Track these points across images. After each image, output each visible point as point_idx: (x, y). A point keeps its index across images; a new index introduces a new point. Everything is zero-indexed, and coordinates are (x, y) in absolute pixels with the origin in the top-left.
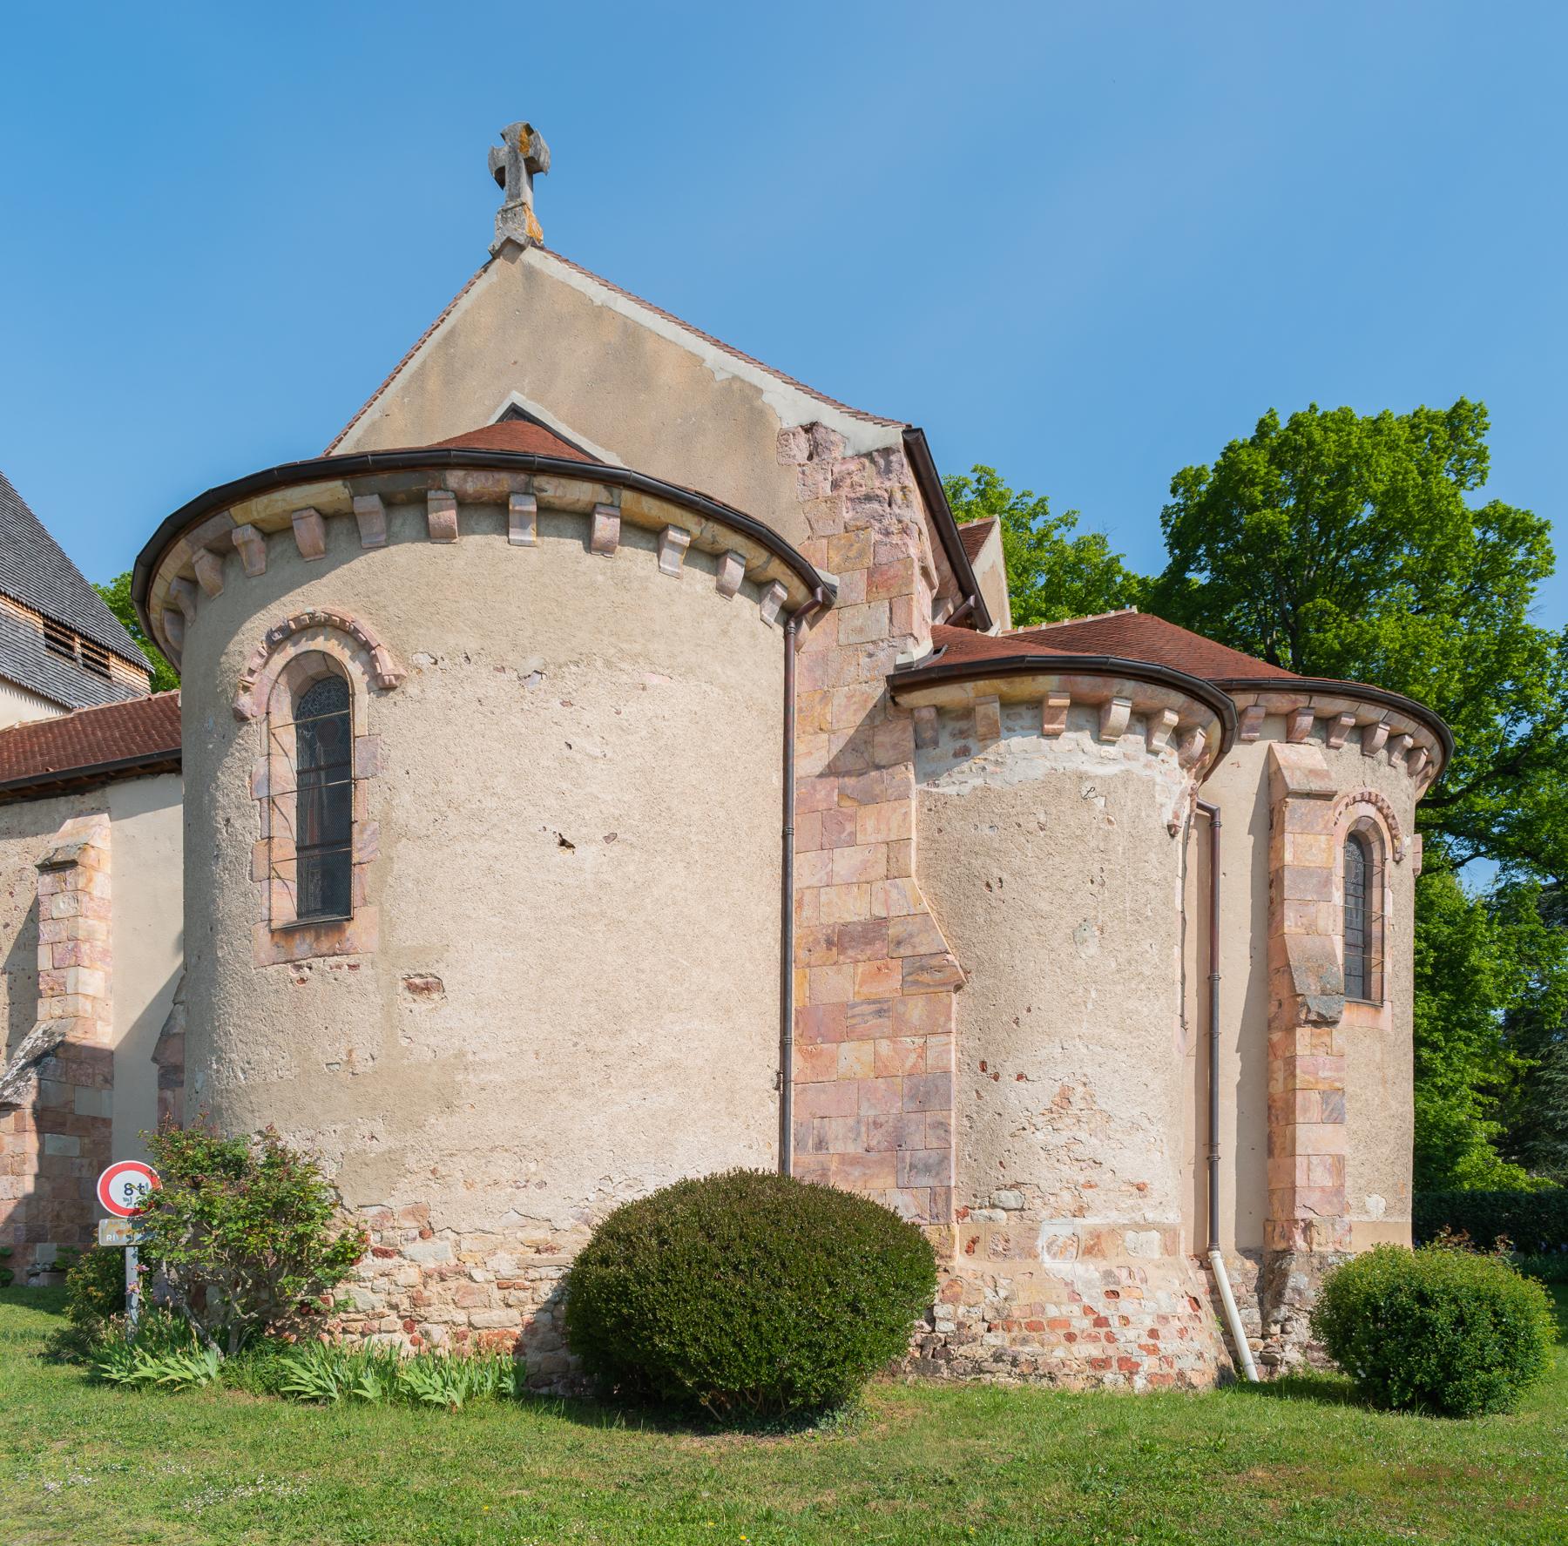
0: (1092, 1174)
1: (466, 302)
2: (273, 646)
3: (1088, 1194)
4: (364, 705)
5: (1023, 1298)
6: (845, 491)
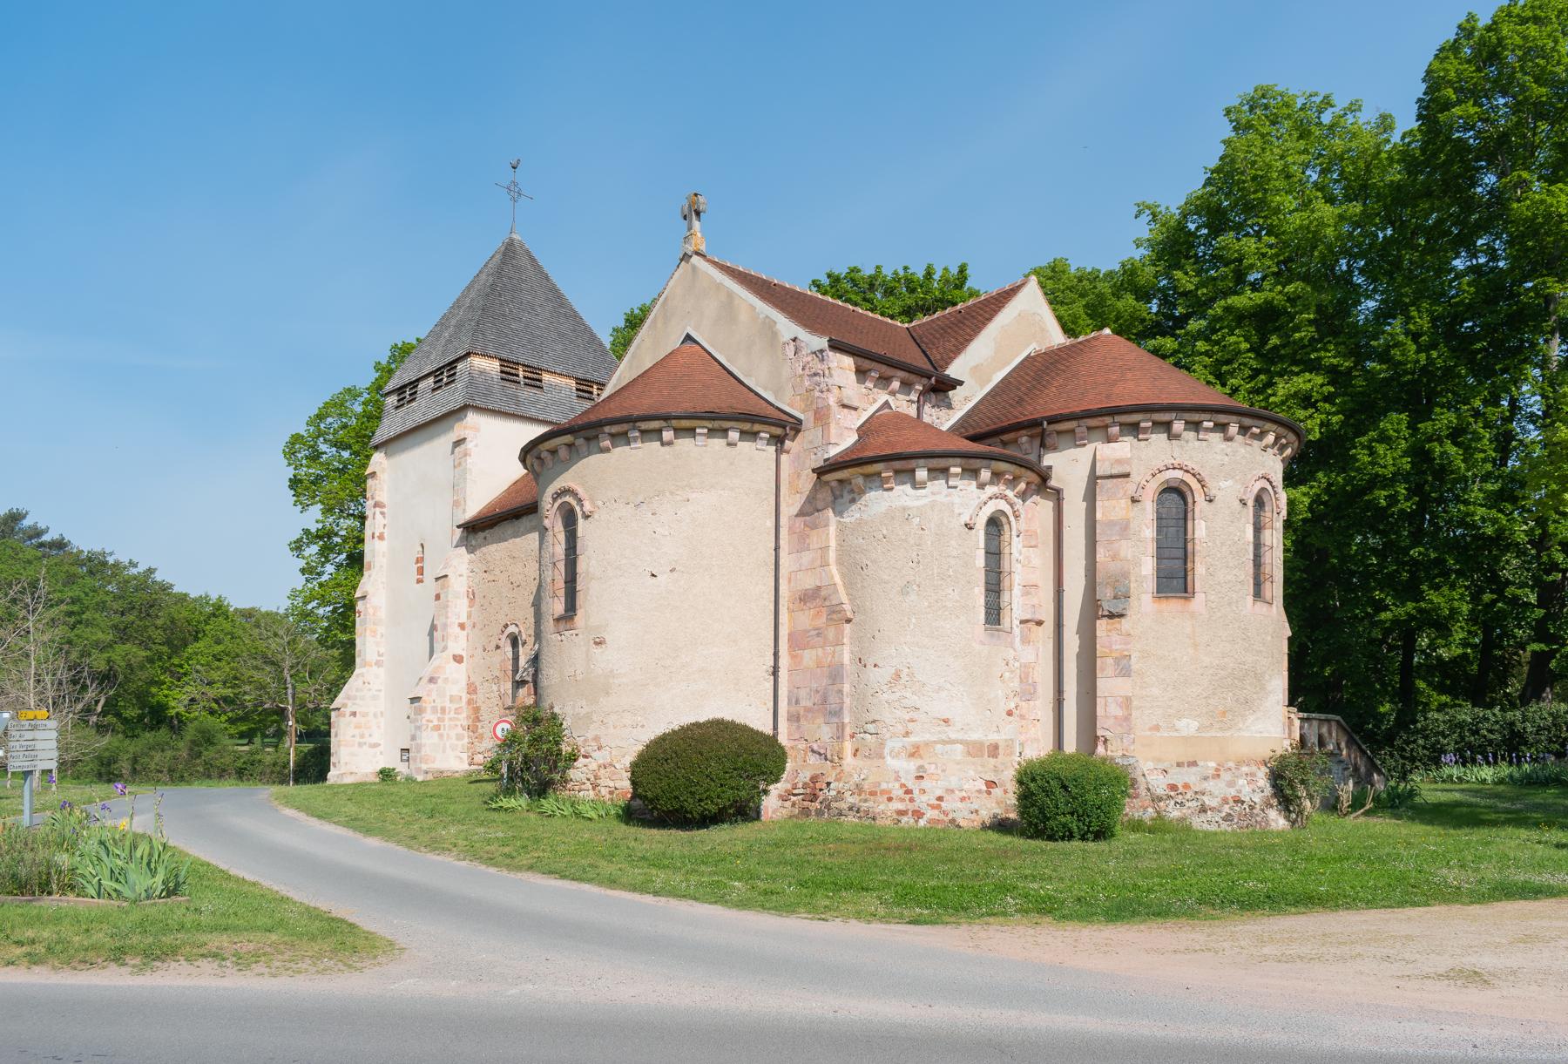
0: (914, 715)
1: (671, 283)
2: (555, 500)
3: (910, 725)
4: (581, 521)
5: (871, 779)
6: (807, 372)
